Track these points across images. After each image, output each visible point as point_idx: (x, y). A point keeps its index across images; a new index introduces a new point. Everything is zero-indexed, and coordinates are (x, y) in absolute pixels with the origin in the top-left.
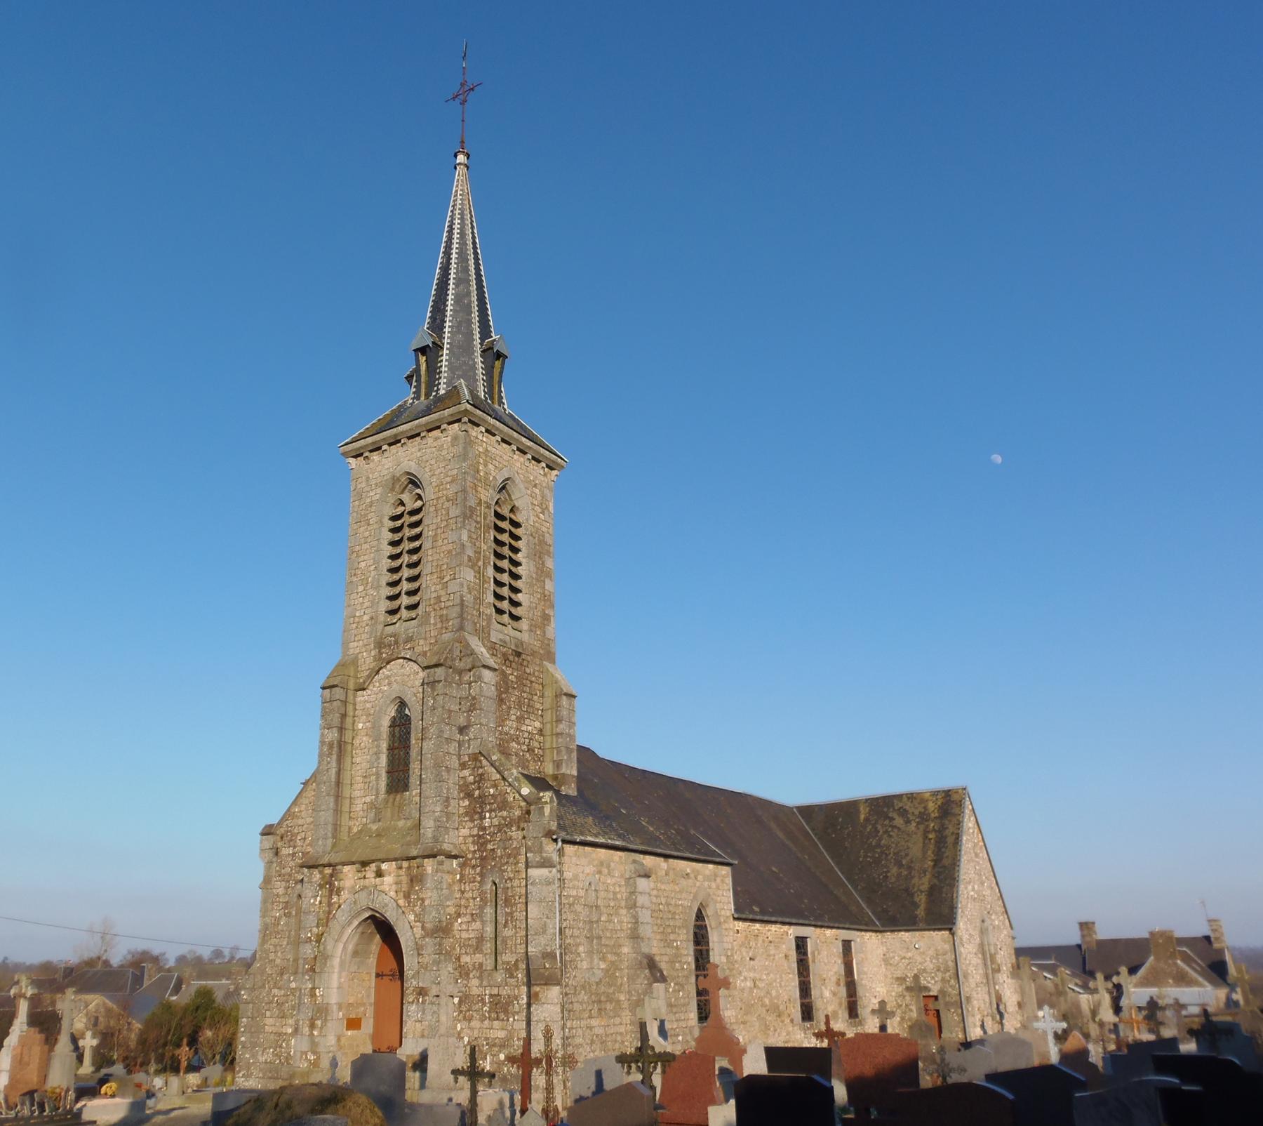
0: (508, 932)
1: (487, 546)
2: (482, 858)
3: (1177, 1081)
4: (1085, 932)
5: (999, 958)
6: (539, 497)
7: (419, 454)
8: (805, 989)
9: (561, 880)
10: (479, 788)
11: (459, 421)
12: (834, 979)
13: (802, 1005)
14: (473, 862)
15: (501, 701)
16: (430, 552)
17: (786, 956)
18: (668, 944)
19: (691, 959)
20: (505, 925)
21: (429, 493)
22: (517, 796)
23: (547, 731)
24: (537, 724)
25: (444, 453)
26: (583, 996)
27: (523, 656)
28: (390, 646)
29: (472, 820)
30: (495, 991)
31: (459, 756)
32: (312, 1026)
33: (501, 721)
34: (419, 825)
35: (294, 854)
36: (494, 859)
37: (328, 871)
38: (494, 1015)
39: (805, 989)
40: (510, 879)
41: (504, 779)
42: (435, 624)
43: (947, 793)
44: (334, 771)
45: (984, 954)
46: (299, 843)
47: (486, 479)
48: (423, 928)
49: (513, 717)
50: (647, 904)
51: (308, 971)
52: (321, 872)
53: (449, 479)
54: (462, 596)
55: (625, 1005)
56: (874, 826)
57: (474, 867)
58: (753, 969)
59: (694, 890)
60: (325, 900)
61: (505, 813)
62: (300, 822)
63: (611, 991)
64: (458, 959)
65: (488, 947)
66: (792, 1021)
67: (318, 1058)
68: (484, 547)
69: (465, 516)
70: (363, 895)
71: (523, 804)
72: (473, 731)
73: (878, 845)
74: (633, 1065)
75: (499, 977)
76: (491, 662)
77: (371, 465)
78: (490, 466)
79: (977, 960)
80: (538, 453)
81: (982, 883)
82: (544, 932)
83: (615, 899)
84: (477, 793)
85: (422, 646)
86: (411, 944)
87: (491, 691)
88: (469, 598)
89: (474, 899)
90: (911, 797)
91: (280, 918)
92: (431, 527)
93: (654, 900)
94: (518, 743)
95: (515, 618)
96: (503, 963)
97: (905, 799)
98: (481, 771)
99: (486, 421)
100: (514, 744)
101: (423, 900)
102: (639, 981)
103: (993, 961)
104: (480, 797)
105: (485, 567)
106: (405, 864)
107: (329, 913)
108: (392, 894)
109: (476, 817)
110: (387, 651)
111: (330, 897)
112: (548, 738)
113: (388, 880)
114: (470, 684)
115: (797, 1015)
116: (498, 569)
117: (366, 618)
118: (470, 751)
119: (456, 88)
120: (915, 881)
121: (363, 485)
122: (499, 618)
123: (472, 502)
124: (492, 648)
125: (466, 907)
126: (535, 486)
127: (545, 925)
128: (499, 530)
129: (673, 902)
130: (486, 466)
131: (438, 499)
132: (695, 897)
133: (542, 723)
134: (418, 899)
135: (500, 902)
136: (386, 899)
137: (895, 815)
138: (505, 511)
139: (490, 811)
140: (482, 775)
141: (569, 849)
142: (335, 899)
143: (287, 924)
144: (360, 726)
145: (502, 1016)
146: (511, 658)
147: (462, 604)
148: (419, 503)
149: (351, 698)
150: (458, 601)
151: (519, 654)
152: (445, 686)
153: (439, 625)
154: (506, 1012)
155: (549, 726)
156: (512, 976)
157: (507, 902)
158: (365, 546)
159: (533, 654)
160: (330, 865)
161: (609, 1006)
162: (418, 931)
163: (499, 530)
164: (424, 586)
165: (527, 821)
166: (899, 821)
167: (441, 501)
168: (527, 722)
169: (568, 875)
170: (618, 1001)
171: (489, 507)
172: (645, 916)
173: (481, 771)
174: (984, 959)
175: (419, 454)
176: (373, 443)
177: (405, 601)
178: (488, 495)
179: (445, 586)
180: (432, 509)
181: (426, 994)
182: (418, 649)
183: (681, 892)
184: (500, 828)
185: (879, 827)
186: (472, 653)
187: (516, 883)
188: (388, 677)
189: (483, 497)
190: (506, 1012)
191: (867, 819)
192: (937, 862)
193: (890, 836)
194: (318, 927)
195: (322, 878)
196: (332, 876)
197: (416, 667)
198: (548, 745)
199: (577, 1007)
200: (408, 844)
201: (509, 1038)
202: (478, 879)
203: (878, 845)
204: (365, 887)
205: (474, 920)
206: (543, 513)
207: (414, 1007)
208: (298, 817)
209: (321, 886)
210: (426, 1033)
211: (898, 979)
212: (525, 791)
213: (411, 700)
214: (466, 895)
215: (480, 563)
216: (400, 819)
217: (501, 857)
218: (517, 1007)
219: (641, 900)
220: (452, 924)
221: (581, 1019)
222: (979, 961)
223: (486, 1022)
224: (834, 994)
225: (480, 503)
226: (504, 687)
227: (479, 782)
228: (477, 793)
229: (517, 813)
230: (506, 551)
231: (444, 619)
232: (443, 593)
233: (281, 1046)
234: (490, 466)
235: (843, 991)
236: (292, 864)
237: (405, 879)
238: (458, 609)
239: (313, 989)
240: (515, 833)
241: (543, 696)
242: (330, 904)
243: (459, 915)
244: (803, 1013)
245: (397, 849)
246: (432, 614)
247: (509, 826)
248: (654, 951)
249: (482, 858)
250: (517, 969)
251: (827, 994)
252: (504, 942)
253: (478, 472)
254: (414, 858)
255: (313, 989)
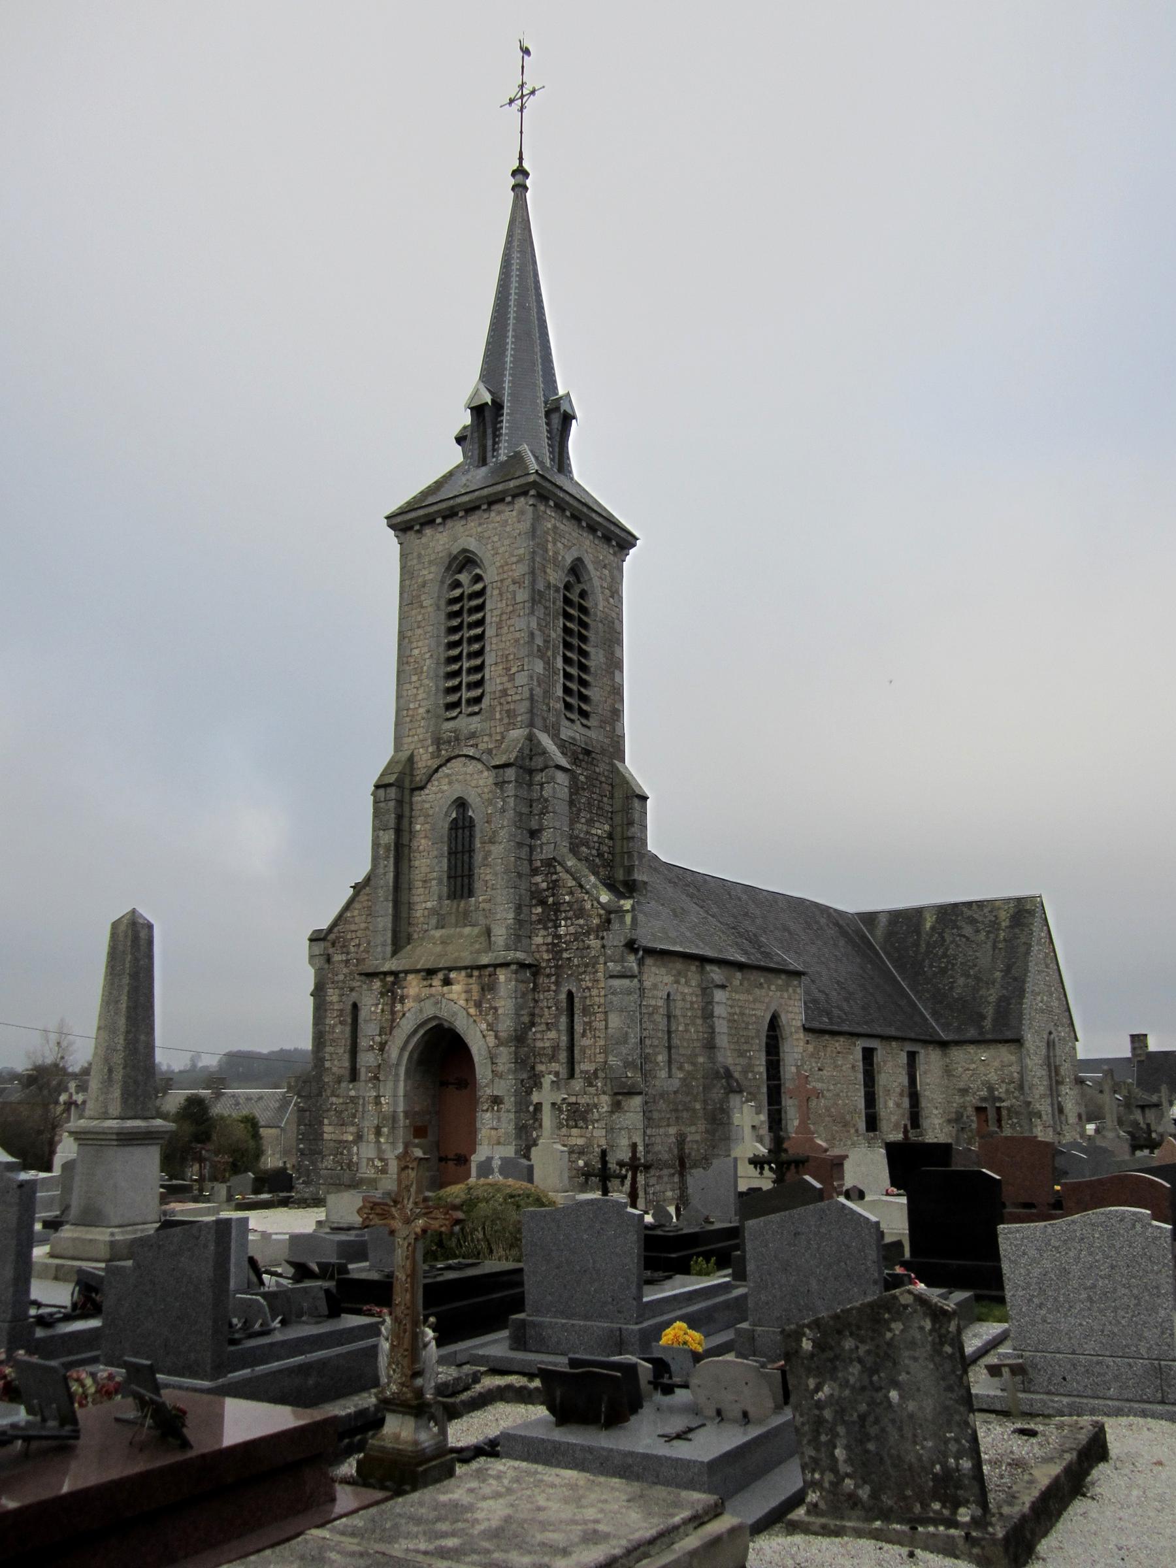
0: (586, 1042)
1: (556, 634)
2: (557, 967)
3: (249, 1370)
4: (1137, 1045)
5: (1062, 1072)
6: (609, 579)
7: (479, 529)
8: (871, 1100)
9: (642, 990)
10: (553, 895)
11: (525, 494)
12: (898, 1090)
13: (867, 1115)
14: (548, 971)
15: (571, 803)
16: (494, 640)
17: (853, 1067)
18: (741, 1054)
19: (763, 1069)
20: (584, 1035)
21: (491, 575)
22: (595, 904)
23: (618, 836)
24: (607, 827)
25: (508, 529)
26: (662, 1105)
27: (593, 755)
28: (449, 742)
29: (546, 928)
30: (573, 1099)
31: (531, 861)
32: (378, 1133)
33: (572, 822)
34: (488, 932)
35: (347, 961)
36: (570, 968)
37: (390, 979)
38: (571, 1123)
39: (871, 1100)
40: (588, 988)
41: (581, 886)
42: (501, 720)
43: (1019, 901)
44: (391, 875)
45: (1049, 1066)
46: (352, 949)
47: (555, 558)
48: (496, 1037)
49: (583, 820)
50: (724, 1015)
51: (371, 1079)
52: (381, 980)
53: (514, 559)
54: (531, 690)
55: (700, 1114)
56: (941, 935)
57: (549, 976)
58: (821, 1080)
59: (767, 1000)
60: (387, 1008)
61: (581, 922)
62: (353, 927)
63: (688, 1099)
64: (533, 1068)
65: (563, 1056)
66: (857, 1131)
67: (387, 1165)
68: (553, 635)
69: (533, 601)
70: (428, 1003)
71: (602, 912)
72: (546, 836)
73: (945, 955)
74: (766, 1167)
75: (577, 1084)
76: (563, 762)
77: (424, 540)
78: (559, 545)
79: (1042, 1072)
80: (608, 529)
81: (1051, 994)
82: (626, 1042)
83: (692, 1008)
84: (551, 900)
85: (485, 743)
86: (484, 1052)
87: (564, 793)
88: (538, 691)
89: (549, 1008)
90: (980, 904)
91: (334, 1026)
92: (495, 613)
93: (729, 1010)
94: (588, 848)
95: (584, 714)
96: (581, 1072)
97: (974, 907)
98: (555, 877)
99: (555, 494)
100: (584, 849)
101: (496, 1009)
102: (715, 1091)
103: (1057, 1074)
104: (554, 904)
105: (555, 658)
106: (476, 973)
107: (393, 1020)
108: (462, 1003)
109: (550, 925)
110: (447, 750)
111: (393, 1005)
112: (618, 843)
113: (456, 988)
114: (542, 785)
115: (862, 1126)
116: (567, 660)
117: (421, 710)
118: (543, 857)
119: (513, 92)
120: (983, 992)
121: (415, 561)
122: (569, 715)
123: (541, 586)
124: (563, 745)
125: (541, 1016)
126: (605, 567)
127: (627, 1033)
128: (567, 616)
129: (747, 1011)
130: (555, 544)
131: (502, 581)
132: (768, 1008)
133: (611, 826)
134: (491, 1008)
135: (577, 1011)
136: (456, 1008)
137: (963, 924)
138: (575, 598)
139: (566, 919)
140: (557, 881)
141: (649, 961)
142: (398, 1007)
143: (342, 1032)
144: (418, 827)
145: (581, 1123)
146: (581, 757)
147: (531, 698)
148: (479, 587)
149: (407, 798)
150: (527, 694)
151: (588, 753)
152: (516, 787)
153: (506, 721)
154: (585, 1120)
155: (619, 829)
156: (591, 1085)
157: (586, 1011)
158: (420, 631)
159: (603, 752)
160: (392, 973)
161: (685, 1115)
162: (491, 1041)
163: (567, 616)
164: (487, 677)
165: (608, 929)
166: (968, 930)
167: (506, 583)
168: (597, 825)
169: (647, 984)
170: (694, 1110)
171: (557, 590)
172: (721, 1027)
173: (555, 877)
174: (1050, 1071)
175: (479, 529)
176: (426, 515)
177: (466, 694)
178: (557, 577)
179: (512, 678)
180: (496, 592)
181: (502, 1102)
182: (482, 746)
183: (754, 1001)
184: (576, 936)
185: (946, 935)
186: (544, 752)
187: (594, 992)
188: (448, 776)
189: (552, 581)
190: (585, 1120)
191: (933, 928)
192: (1008, 970)
193: (958, 946)
194: (380, 1035)
195: (383, 986)
196: (394, 983)
197: (480, 766)
198: (618, 850)
199: (656, 1115)
200: (478, 952)
201: (589, 1145)
202: (553, 987)
203: (945, 955)
204: (432, 995)
205: (549, 1029)
206: (612, 597)
207: (488, 1115)
208: (351, 923)
209: (382, 994)
210: (502, 1140)
211: (960, 1090)
212: (605, 898)
213: (473, 799)
214: (541, 1004)
215: (550, 653)
216: (465, 925)
217: (578, 966)
218: (596, 1116)
219: (719, 1010)
220: (526, 1034)
221: (660, 1127)
222: (1044, 1073)
223: (564, 1130)
224: (898, 1105)
225: (548, 586)
226: (575, 788)
227: (553, 889)
228: (551, 900)
229: (596, 921)
230: (575, 641)
231: (511, 714)
232: (509, 685)
233: (342, 1154)
234: (559, 545)
235: (906, 1102)
236: (345, 971)
237: (475, 988)
238: (527, 704)
239: (378, 1097)
240: (594, 942)
241: (612, 797)
242: (393, 1013)
243: (533, 1024)
244: (867, 1122)
245: (467, 959)
246: (498, 709)
247: (587, 934)
248: (730, 1061)
249: (557, 967)
250: (597, 1078)
251: (891, 1104)
252: (583, 1050)
253: (546, 551)
254: (485, 966)
255: (378, 1097)
